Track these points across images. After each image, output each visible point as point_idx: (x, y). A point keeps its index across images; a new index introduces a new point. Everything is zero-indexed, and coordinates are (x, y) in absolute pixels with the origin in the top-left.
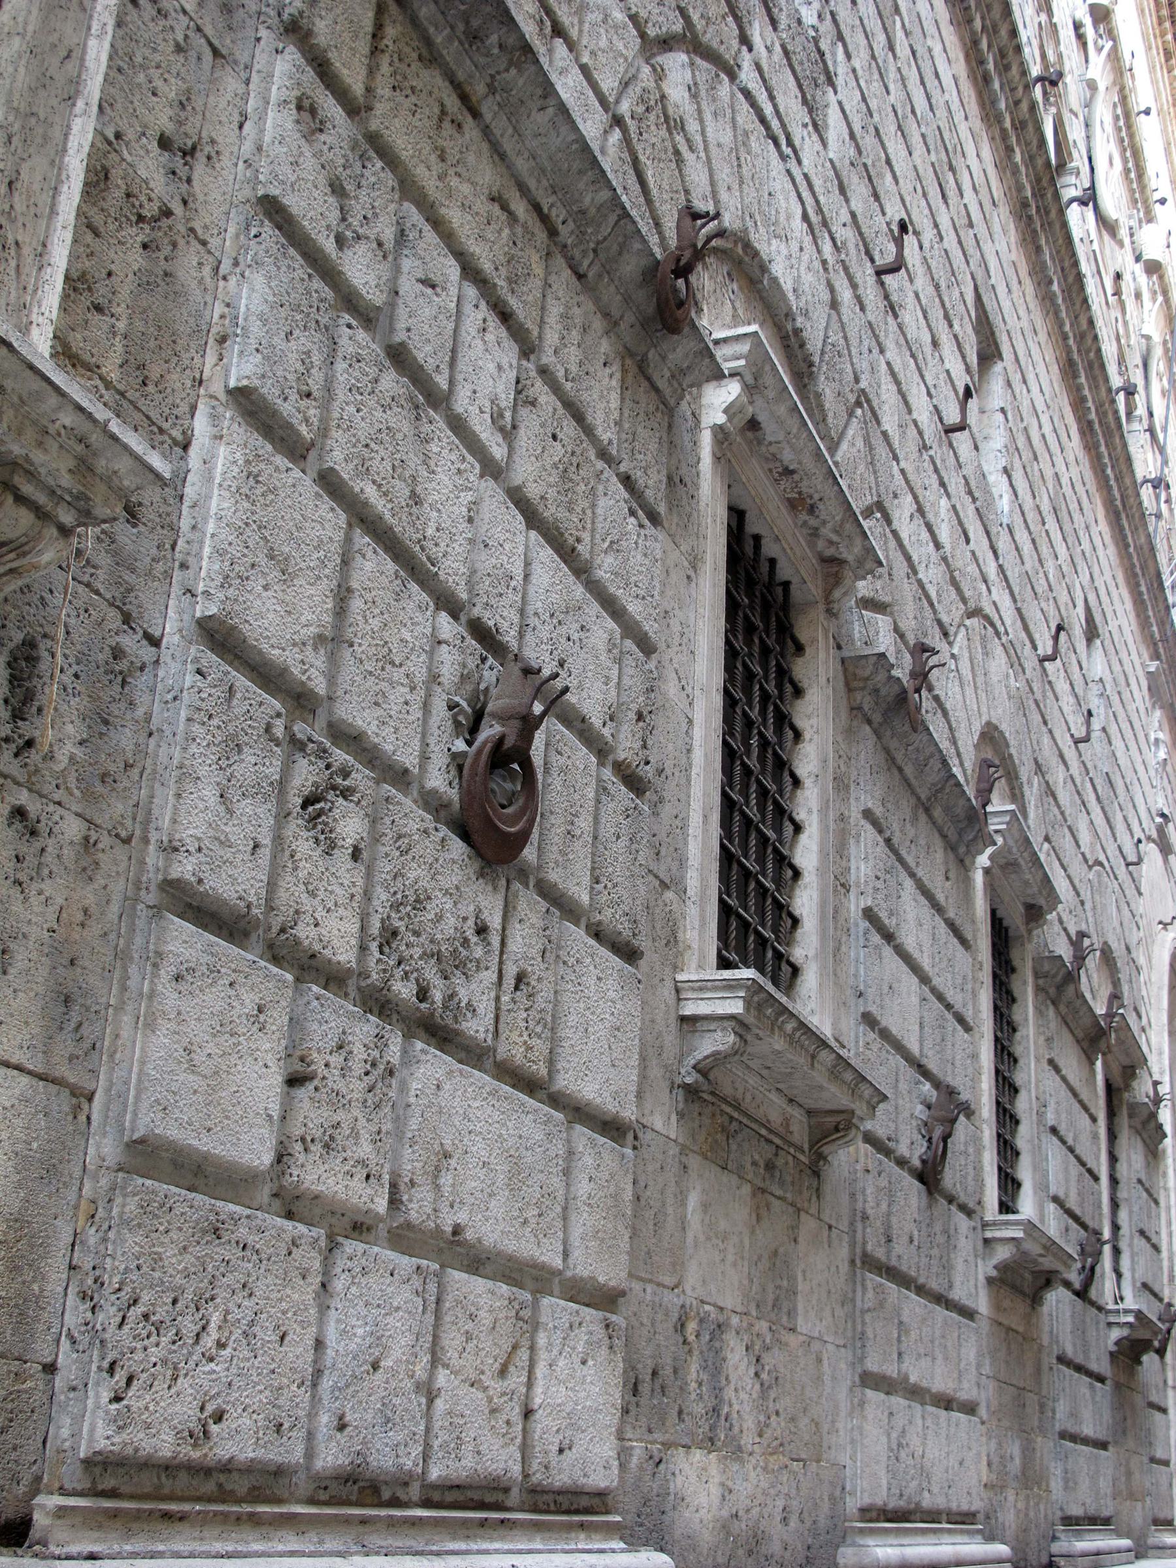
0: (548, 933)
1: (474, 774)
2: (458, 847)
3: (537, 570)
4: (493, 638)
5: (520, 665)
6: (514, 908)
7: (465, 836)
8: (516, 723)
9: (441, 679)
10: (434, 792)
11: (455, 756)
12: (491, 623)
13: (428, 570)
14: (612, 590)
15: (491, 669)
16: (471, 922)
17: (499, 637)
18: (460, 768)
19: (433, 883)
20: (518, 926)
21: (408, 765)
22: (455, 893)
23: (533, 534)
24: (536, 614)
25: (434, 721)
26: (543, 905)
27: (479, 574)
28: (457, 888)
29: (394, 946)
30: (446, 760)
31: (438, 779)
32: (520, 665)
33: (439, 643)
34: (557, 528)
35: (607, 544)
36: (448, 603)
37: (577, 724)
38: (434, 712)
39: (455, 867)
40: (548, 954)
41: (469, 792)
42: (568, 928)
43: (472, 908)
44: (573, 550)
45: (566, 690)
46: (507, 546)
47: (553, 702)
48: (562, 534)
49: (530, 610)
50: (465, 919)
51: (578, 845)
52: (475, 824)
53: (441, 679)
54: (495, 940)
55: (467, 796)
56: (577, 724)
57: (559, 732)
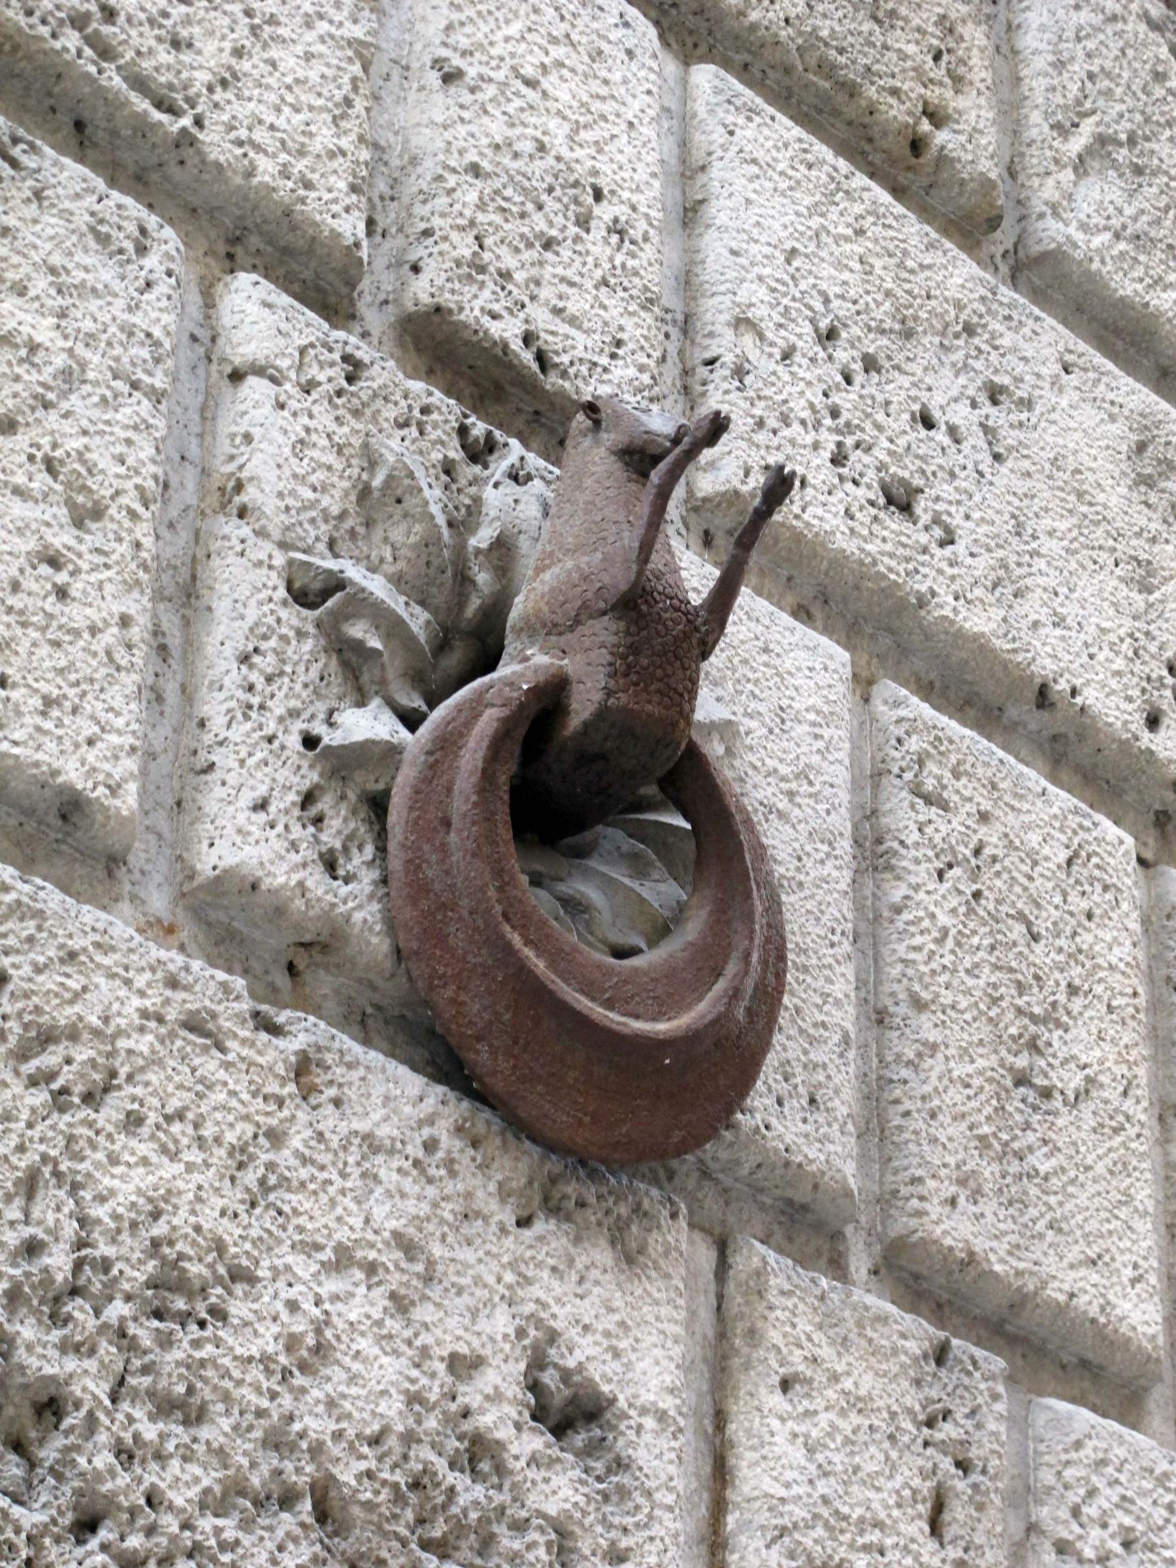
0: (947, 1431)
1: (433, 822)
2: (392, 1095)
3: (729, 189)
4: (529, 386)
5: (609, 438)
6: (752, 1334)
7: (447, 1065)
8: (604, 632)
9: (251, 495)
10: (245, 887)
11: (343, 764)
12: (508, 330)
13: (143, 128)
14: (1127, 287)
15: (516, 477)
16: (503, 1376)
17: (552, 381)
18: (377, 806)
19: (262, 1222)
20: (776, 1400)
21: (73, 774)
22: (409, 1271)
23: (705, 75)
24: (742, 323)
25: (224, 635)
26: (914, 1332)
27: (429, 167)
28: (407, 1247)
29: (49, 1454)
30: (295, 774)
31: (251, 833)
32: (609, 438)
33: (236, 377)
34: (826, 68)
35: (1077, 144)
36: (247, 234)
37: (1021, 710)
38: (222, 607)
39: (387, 1170)
40: (957, 1513)
41: (419, 889)
42: (1057, 1422)
43: (501, 1323)
44: (917, 145)
45: (780, 485)
46: (562, 90)
47: (749, 535)
48: (852, 90)
49: (715, 312)
50: (463, 1366)
51: (1073, 1126)
52: (474, 1008)
53: (251, 495)
54: (660, 1458)
55: (418, 904)
56: (1021, 710)
57: (913, 726)
